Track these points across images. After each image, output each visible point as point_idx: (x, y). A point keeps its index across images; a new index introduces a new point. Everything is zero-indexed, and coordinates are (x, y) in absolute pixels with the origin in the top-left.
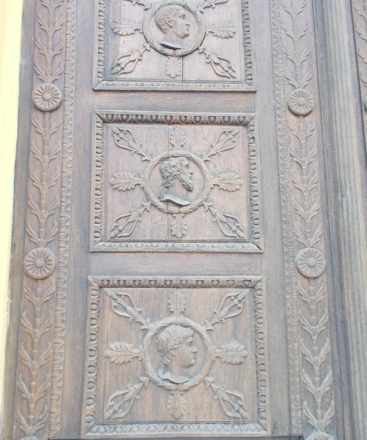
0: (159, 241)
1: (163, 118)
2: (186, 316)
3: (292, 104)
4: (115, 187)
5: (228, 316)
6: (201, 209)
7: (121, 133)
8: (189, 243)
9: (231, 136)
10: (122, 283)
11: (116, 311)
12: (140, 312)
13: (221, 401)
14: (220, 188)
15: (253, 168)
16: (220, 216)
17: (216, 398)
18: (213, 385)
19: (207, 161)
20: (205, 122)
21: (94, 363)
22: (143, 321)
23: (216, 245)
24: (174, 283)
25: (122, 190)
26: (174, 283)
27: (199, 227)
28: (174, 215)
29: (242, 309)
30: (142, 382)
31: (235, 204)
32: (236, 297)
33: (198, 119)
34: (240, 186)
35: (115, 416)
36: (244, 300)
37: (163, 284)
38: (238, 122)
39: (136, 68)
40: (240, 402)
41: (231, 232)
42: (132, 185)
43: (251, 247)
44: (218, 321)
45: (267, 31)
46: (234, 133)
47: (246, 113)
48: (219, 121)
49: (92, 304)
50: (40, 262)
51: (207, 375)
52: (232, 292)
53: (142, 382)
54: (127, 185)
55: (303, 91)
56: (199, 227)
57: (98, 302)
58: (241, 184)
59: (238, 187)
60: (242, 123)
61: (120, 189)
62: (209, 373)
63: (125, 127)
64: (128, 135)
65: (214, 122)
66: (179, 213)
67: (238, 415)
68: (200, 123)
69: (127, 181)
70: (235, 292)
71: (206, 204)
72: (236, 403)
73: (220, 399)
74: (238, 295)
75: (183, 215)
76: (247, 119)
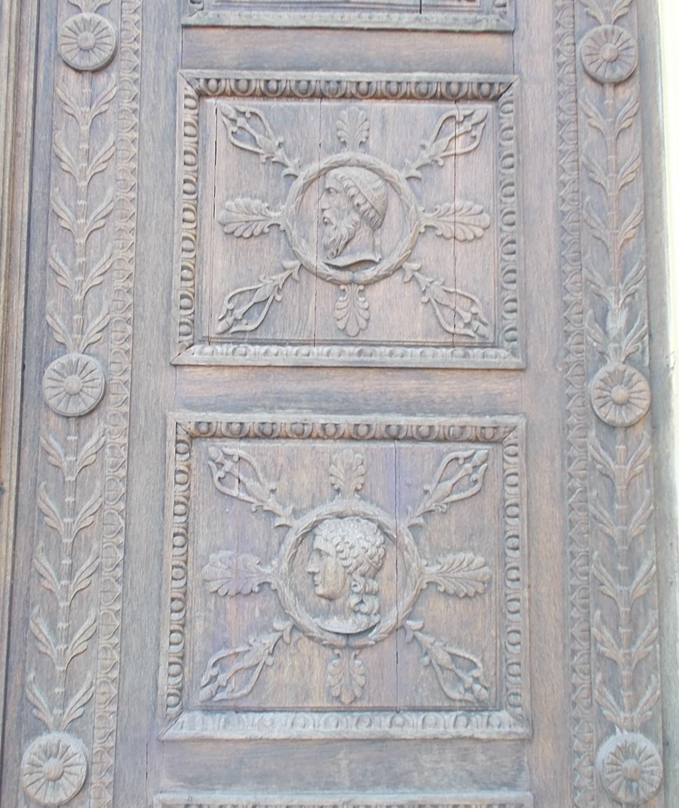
0: (315, 343)
1: (262, 85)
2: (363, 498)
6: (397, 277)
8: (405, 349)
9: (468, 125)
12: (273, 491)
13: (438, 669)
14: (439, 233)
16: (437, 290)
18: (419, 635)
20: (318, 93)
22: (278, 509)
25: (241, 236)
26: (247, 427)
27: (395, 313)
28: (342, 287)
30: (278, 631)
31: (471, 270)
32: (468, 459)
33: (454, 88)
34: (484, 229)
35: (219, 696)
36: (486, 465)
37: (223, 429)
38: (385, 94)
40: (475, 673)
46: (475, 119)
47: (433, 75)
48: (288, 88)
51: (409, 617)
52: (462, 451)
53: (278, 631)
54: (254, 226)
55: (83, 19)
56: (395, 313)
57: (189, 467)
59: (479, 232)
60: (307, 93)
62: (411, 612)
64: (254, 120)
65: (488, 96)
66: (352, 282)
67: (469, 696)
68: (399, 96)
71: (406, 265)
74: (472, 114)
75: (361, 287)
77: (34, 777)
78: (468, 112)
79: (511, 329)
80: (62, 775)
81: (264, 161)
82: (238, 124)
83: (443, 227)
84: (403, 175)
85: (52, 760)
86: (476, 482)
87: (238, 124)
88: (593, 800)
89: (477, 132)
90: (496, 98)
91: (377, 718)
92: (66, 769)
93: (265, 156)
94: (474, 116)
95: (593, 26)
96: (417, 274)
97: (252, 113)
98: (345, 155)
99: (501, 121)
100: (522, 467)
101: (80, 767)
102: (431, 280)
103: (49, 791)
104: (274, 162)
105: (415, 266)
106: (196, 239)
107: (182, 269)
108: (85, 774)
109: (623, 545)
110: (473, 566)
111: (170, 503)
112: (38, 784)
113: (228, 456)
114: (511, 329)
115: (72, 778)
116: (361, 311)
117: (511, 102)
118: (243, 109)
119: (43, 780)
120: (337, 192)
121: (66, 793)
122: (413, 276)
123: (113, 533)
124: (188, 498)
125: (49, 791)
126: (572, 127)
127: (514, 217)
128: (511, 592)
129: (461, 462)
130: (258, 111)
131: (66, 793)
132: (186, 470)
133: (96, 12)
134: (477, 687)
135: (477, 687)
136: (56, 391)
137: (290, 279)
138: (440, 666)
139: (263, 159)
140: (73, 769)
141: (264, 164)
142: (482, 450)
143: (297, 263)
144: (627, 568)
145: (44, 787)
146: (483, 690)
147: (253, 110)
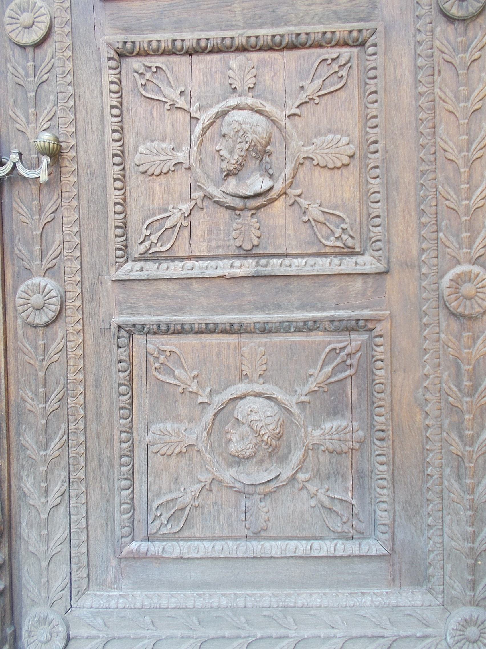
3: (447, 6)
4: (142, 168)
5: (332, 380)
7: (147, 71)
9: (335, 67)
10: (163, 328)
11: (160, 377)
14: (315, 162)
15: (377, 248)
16: (315, 212)
17: (306, 219)
19: (294, 115)
21: (119, 150)
23: (311, 260)
24: (237, 42)
29: (345, 78)
39: (176, 244)
41: (332, 238)
42: (170, 165)
43: (367, 263)
44: (307, 100)
45: (408, 77)
49: (115, 180)
50: (36, 299)
52: (331, 53)
58: (352, 154)
61: (150, 172)
63: (153, 62)
67: (339, 244)
69: (162, 158)
70: (341, 342)
71: (289, 191)
72: (337, 226)
73: (311, 219)
74: (338, 57)
76: (365, 34)
77: (14, 26)
78: (334, 56)
79: (373, 117)
80: (33, 24)
81: (169, 108)
82: (147, 77)
83: (319, 157)
84: (294, 400)
85: (25, 14)
86: (351, 365)
87: (147, 77)
88: (431, 23)
89: (343, 72)
90: (363, 44)
91: (271, 261)
92: (36, 20)
93: (169, 104)
94: (341, 58)
95: (454, 266)
96: (298, 199)
97: (156, 67)
98: (234, 101)
99: (367, 87)
100: (385, 236)
101: (45, 16)
102: (310, 203)
103: (26, 35)
104: (176, 108)
105: (298, 192)
106: (123, 179)
107: (114, 181)
108: (49, 21)
109: (464, 119)
110: (340, 144)
111: (111, 203)
112: (17, 31)
113: (161, 352)
114: (373, 117)
115: (39, 25)
116: (253, 230)
117: (381, 336)
118: (149, 65)
119: (20, 28)
120: (243, 424)
121: (36, 35)
122: (295, 200)
123: (65, 124)
124: (124, 176)
125: (26, 35)
126: (431, 176)
127: (378, 170)
128: (378, 354)
129: (329, 62)
130: (161, 65)
131: (36, 35)
132: (122, 202)
133: (44, 277)
134: (345, 237)
135: (345, 237)
136: (14, 26)
137: (196, 207)
138: (315, 220)
139: (167, 106)
140: (40, 19)
141: (169, 110)
142: (346, 52)
143: (201, 194)
144: (471, 384)
145: (22, 33)
146: (350, 239)
147: (158, 65)
